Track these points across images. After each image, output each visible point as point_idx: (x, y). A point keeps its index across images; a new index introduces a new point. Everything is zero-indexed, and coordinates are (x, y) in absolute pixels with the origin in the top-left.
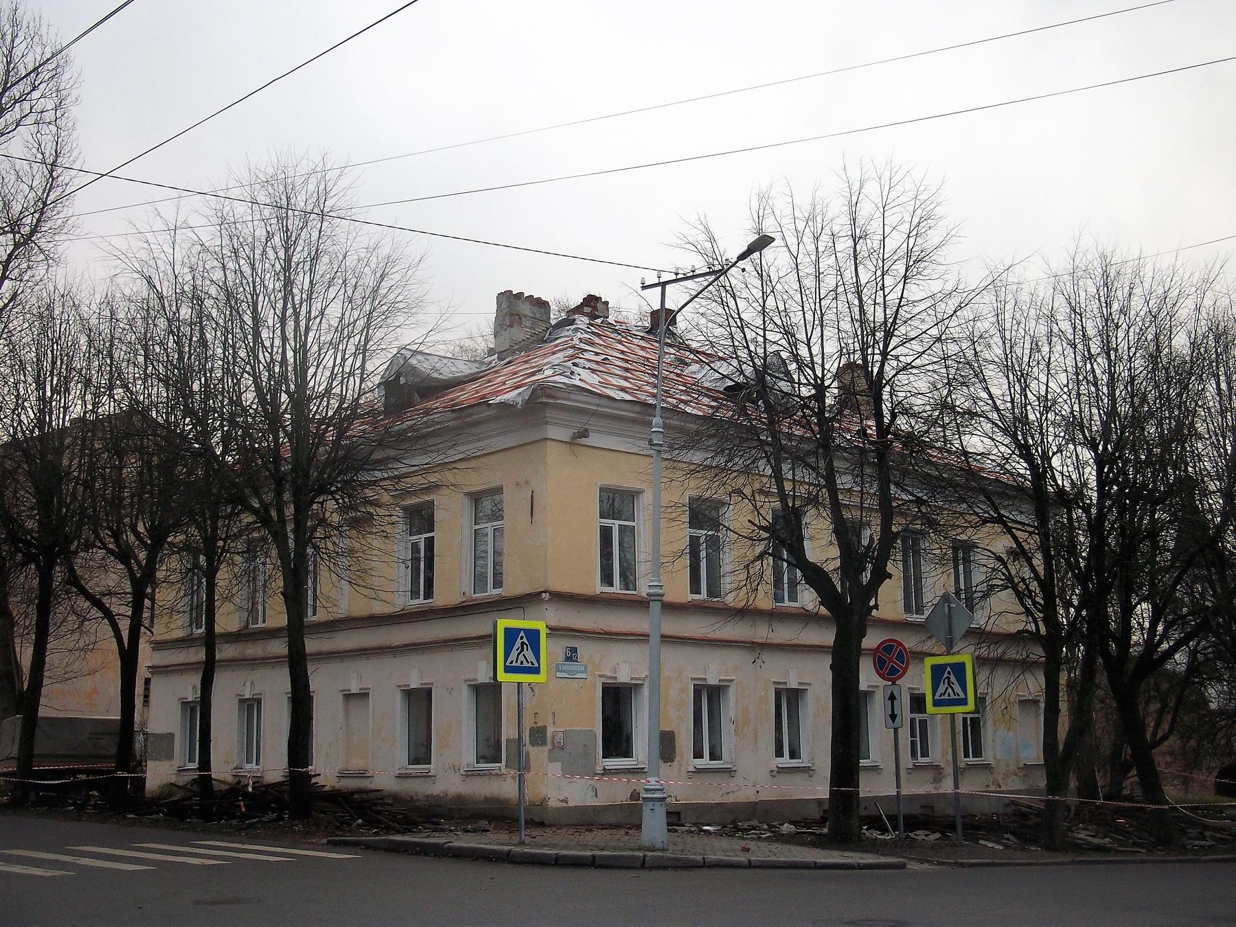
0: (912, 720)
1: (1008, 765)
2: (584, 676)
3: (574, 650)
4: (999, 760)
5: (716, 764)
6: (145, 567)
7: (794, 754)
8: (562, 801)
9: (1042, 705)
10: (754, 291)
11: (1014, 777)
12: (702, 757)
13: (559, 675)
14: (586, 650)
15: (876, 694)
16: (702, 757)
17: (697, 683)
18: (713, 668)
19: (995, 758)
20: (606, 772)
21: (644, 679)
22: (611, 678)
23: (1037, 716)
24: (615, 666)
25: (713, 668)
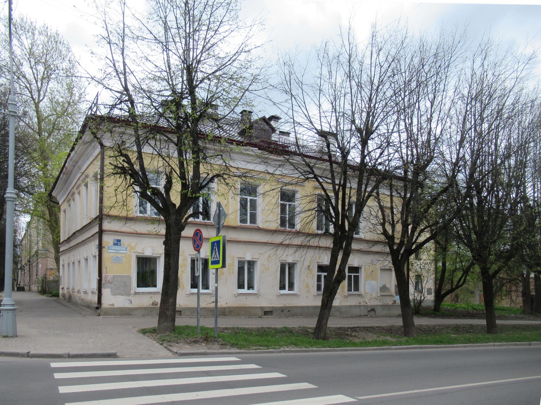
0: (350, 277)
1: (372, 295)
2: (125, 252)
3: (119, 241)
4: (367, 293)
5: (251, 291)
6: (415, 252)
7: (251, 287)
8: (111, 305)
9: (393, 269)
10: (325, 121)
11: (375, 300)
12: (244, 288)
13: (109, 251)
14: (125, 241)
15: (298, 264)
16: (244, 288)
17: (240, 259)
18: (289, 256)
19: (365, 291)
20: (136, 293)
21: (161, 254)
22: (141, 253)
23: (391, 275)
24: (143, 249)
25: (289, 256)
